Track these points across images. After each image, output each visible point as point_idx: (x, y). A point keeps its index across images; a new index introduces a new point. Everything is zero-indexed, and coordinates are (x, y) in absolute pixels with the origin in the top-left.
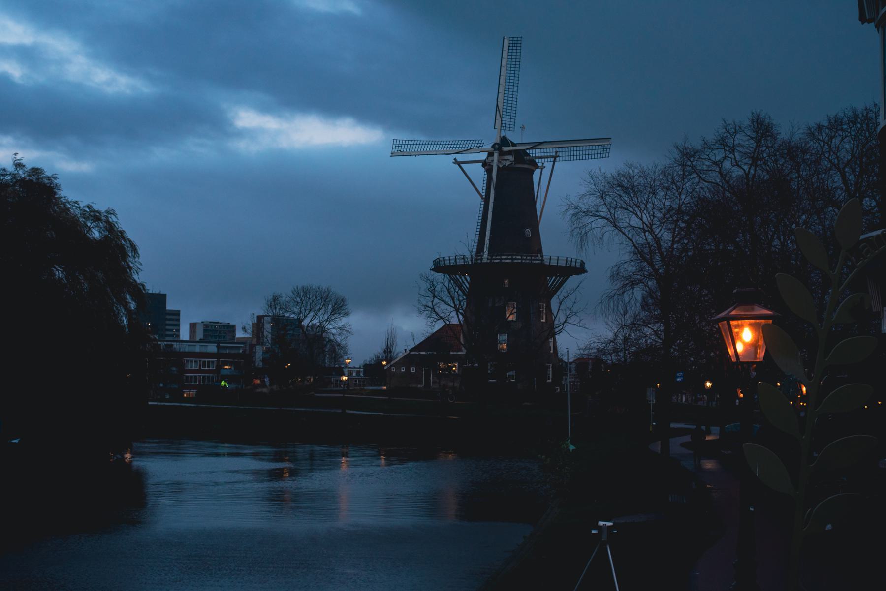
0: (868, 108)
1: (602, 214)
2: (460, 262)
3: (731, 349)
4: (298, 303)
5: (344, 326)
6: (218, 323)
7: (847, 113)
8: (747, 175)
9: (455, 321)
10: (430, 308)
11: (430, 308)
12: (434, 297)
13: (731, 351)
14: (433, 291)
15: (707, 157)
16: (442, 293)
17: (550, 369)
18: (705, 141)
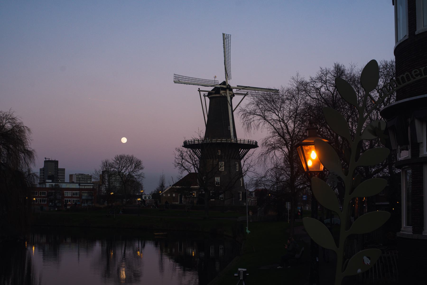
0: (393, 61)
1: (258, 113)
2: (196, 142)
3: (304, 164)
4: (118, 163)
5: (141, 174)
6: (83, 174)
7: (382, 63)
8: (333, 94)
9: (193, 171)
10: (180, 164)
11: (180, 164)
12: (183, 159)
13: (304, 166)
14: (182, 156)
15: (313, 86)
16: (187, 157)
17: (241, 194)
18: (312, 78)
